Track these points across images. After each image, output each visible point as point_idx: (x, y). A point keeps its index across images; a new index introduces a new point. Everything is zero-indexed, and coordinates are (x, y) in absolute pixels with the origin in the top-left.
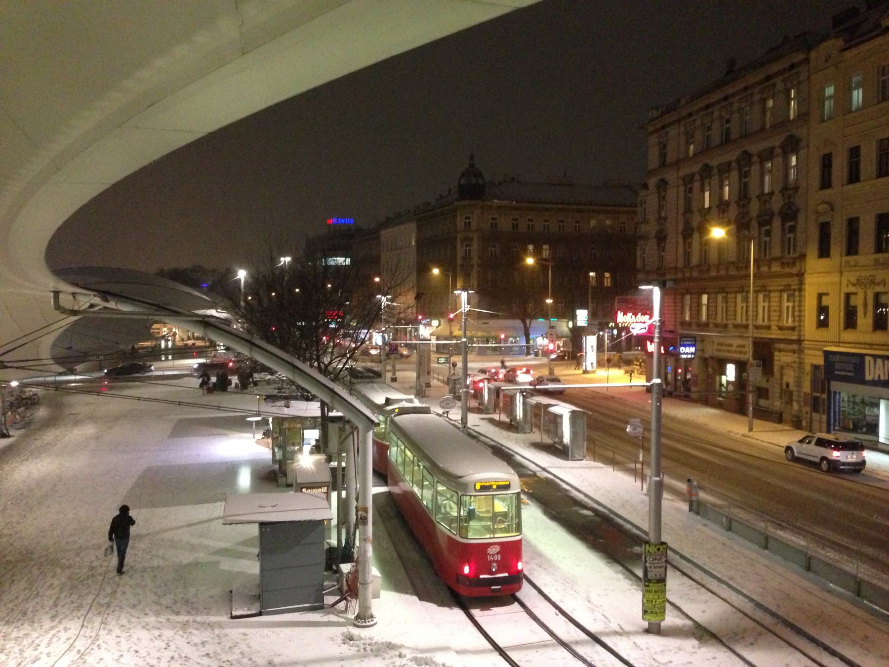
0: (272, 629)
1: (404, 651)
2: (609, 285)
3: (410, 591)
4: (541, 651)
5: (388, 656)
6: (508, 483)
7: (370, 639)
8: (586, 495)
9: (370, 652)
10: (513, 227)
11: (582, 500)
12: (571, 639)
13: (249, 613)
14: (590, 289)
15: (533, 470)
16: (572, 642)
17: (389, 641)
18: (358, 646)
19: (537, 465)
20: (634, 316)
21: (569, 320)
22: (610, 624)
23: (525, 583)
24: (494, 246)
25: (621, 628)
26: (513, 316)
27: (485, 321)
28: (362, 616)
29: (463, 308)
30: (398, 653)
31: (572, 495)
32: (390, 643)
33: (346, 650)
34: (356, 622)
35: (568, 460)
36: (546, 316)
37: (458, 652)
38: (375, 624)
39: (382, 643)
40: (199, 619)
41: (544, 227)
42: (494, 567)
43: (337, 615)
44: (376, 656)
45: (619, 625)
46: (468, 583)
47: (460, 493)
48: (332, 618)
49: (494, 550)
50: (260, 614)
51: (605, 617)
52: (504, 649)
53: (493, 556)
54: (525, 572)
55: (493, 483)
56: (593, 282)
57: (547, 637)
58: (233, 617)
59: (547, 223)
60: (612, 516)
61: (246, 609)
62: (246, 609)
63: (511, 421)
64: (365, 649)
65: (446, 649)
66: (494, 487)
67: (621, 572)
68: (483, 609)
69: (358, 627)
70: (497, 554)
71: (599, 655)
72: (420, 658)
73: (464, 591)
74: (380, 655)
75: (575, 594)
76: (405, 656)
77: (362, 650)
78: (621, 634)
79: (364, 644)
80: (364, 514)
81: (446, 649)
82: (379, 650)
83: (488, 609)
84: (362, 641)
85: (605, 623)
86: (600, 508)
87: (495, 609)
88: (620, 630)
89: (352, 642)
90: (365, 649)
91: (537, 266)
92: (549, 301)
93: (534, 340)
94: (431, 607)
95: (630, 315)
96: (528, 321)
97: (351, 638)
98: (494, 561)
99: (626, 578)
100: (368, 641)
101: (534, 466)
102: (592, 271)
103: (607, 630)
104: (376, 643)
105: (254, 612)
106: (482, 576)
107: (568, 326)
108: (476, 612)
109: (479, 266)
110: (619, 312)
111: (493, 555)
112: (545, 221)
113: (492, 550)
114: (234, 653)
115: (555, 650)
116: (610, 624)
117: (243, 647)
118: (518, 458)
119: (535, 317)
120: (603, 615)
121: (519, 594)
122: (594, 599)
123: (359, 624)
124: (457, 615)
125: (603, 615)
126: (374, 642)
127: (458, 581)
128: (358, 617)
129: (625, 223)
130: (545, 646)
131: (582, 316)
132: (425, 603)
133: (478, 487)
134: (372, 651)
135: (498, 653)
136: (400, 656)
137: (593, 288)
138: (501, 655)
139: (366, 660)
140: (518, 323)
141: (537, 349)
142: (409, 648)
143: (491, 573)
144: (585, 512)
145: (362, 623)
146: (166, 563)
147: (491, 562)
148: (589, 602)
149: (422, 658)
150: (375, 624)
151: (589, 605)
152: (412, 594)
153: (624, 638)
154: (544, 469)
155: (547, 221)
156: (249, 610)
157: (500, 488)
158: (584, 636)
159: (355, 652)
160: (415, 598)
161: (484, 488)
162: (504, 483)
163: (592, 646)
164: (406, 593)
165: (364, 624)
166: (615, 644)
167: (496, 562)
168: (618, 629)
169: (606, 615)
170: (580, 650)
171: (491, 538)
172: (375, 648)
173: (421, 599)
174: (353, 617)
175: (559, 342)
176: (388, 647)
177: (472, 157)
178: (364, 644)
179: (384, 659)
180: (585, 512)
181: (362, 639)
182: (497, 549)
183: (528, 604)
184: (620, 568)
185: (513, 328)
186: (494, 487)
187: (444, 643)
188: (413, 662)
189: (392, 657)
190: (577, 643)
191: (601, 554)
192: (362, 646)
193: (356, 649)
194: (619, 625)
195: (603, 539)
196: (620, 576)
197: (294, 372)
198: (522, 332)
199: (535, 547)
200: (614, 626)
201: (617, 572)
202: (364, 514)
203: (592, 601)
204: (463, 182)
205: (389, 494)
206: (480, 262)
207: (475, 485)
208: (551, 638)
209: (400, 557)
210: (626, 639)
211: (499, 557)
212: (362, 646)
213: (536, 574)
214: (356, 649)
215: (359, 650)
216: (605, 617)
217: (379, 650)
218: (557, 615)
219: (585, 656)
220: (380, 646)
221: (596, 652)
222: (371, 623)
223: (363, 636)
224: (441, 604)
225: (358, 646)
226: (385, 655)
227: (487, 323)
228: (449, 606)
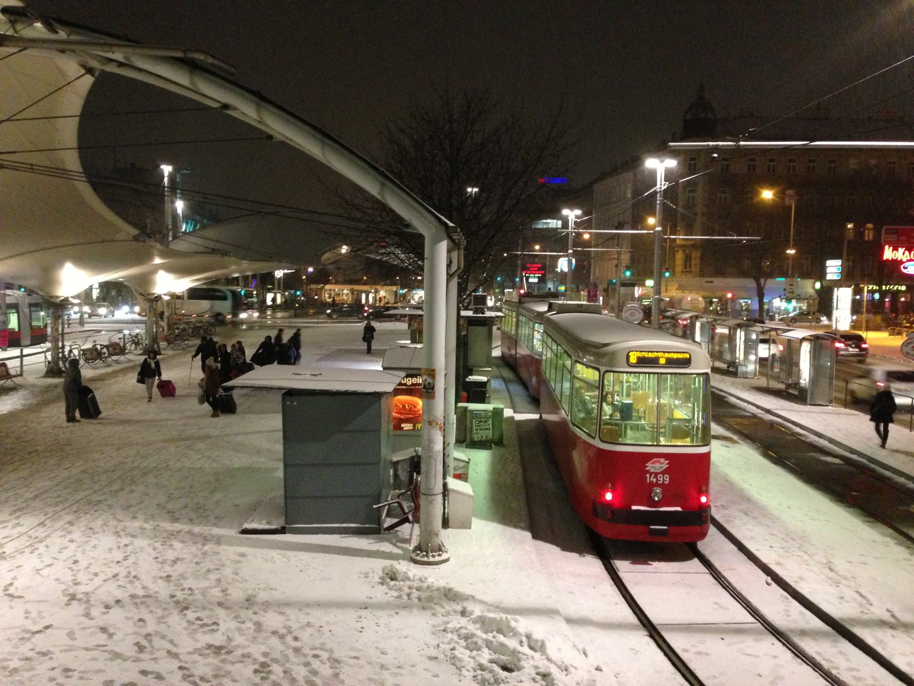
0: (283, 552)
1: (470, 606)
2: (871, 237)
3: (522, 525)
4: (729, 639)
5: (442, 611)
6: (688, 356)
7: (421, 580)
8: (831, 441)
9: (416, 600)
10: (749, 169)
11: (826, 447)
12: (792, 626)
13: (267, 527)
14: (846, 243)
15: (750, 411)
16: (792, 631)
17: (448, 587)
18: (400, 590)
19: (758, 407)
20: (907, 253)
21: (816, 280)
22: (872, 609)
23: (712, 530)
24: (724, 192)
25: (893, 616)
26: (743, 274)
27: (710, 279)
28: (423, 548)
29: (658, 186)
30: (459, 608)
31: (810, 440)
32: (450, 590)
33: (381, 593)
34: (413, 556)
35: (806, 405)
36: (784, 274)
37: (570, 621)
38: (446, 561)
39: (438, 589)
40: (197, 529)
41: (789, 169)
42: (656, 494)
43: (395, 545)
44: (424, 608)
45: (888, 610)
46: (609, 516)
47: (603, 369)
48: (386, 547)
49: (657, 465)
50: (282, 531)
51: (861, 596)
52: (658, 627)
53: (656, 477)
54: (715, 513)
55: (660, 355)
56: (850, 236)
57: (744, 616)
58: (245, 532)
59: (792, 164)
60: (873, 466)
61: (264, 522)
62: (264, 522)
63: (728, 367)
64: (409, 595)
65: (550, 613)
66: (662, 361)
67: (890, 536)
68: (635, 562)
69: (416, 562)
70: (663, 473)
71: (848, 660)
72: (490, 619)
73: (605, 529)
74: (431, 608)
75: (806, 557)
76: (471, 614)
77: (405, 597)
78: (892, 627)
79: (410, 588)
80: (430, 380)
81: (550, 613)
82: (430, 599)
83: (645, 562)
84: (408, 583)
85: (861, 605)
86: (854, 457)
87: (656, 564)
88: (891, 620)
89: (392, 583)
90: (409, 595)
91: (777, 199)
92: (791, 252)
93: (770, 302)
94: (551, 551)
95: (901, 250)
96: (762, 281)
97: (393, 576)
98: (657, 485)
99: (899, 544)
100: (416, 584)
101: (754, 408)
102: (850, 222)
103: (865, 617)
104: (428, 587)
105: (274, 527)
106: (634, 508)
107: (814, 287)
108: (623, 567)
109: (703, 214)
110: (887, 247)
111: (656, 475)
112: (790, 161)
113: (653, 466)
114: (209, 579)
115: (757, 640)
116: (872, 609)
117: (228, 572)
118: (733, 400)
119: (771, 275)
120: (858, 592)
121: (701, 546)
122: (841, 565)
123: (418, 558)
124: (592, 565)
125: (858, 592)
126: (425, 585)
127: (595, 513)
128: (418, 548)
129: (894, 163)
130: (739, 630)
131: (834, 268)
132: (541, 544)
133: (633, 360)
134: (419, 599)
135: (646, 633)
136: (463, 613)
137: (849, 242)
138: (651, 636)
139: (403, 613)
140: (751, 283)
141: (773, 312)
142: (481, 602)
143: (653, 504)
144: (829, 459)
145: (423, 556)
146: (215, 465)
147: (652, 485)
148: (831, 570)
149: (493, 620)
150: (446, 561)
151: (831, 574)
152: (523, 529)
153: (899, 634)
154: (768, 411)
155: (793, 161)
156: (268, 523)
157: (671, 362)
158: (816, 623)
159: (392, 599)
160: (528, 535)
161: (642, 362)
162: (680, 356)
163: (835, 641)
164: (516, 527)
165: (425, 559)
166: (881, 642)
167: (662, 486)
168: (887, 617)
169: (864, 594)
170: (809, 646)
171: (653, 445)
172: (424, 595)
173: (535, 537)
174: (411, 548)
175: (802, 305)
176: (446, 595)
177: (702, 87)
178: (410, 588)
179: (434, 614)
180: (829, 459)
181: (408, 579)
182: (664, 464)
183: (717, 564)
184: (891, 531)
185: (744, 288)
186: (662, 361)
187: (550, 603)
188: (478, 626)
189: (448, 613)
190: (803, 633)
191: (856, 510)
192: (407, 590)
193: (395, 594)
194: (888, 610)
195: (858, 491)
196: (891, 542)
197: (323, 143)
198: (754, 293)
199: (742, 490)
200: (878, 611)
201: (884, 535)
202: (430, 380)
203: (837, 569)
204: (689, 116)
205: (541, 423)
206: (705, 210)
207: (628, 357)
208: (754, 620)
209: (527, 484)
210: (904, 636)
211: (667, 479)
212: (407, 590)
213: (737, 522)
214: (395, 594)
215: (399, 597)
216: (861, 596)
217: (430, 599)
218: (768, 584)
219: (818, 659)
220: (436, 594)
221: (841, 653)
222: (437, 559)
223: (411, 575)
224: (567, 546)
225: (400, 590)
226: (439, 609)
227: (712, 282)
228: (581, 551)
